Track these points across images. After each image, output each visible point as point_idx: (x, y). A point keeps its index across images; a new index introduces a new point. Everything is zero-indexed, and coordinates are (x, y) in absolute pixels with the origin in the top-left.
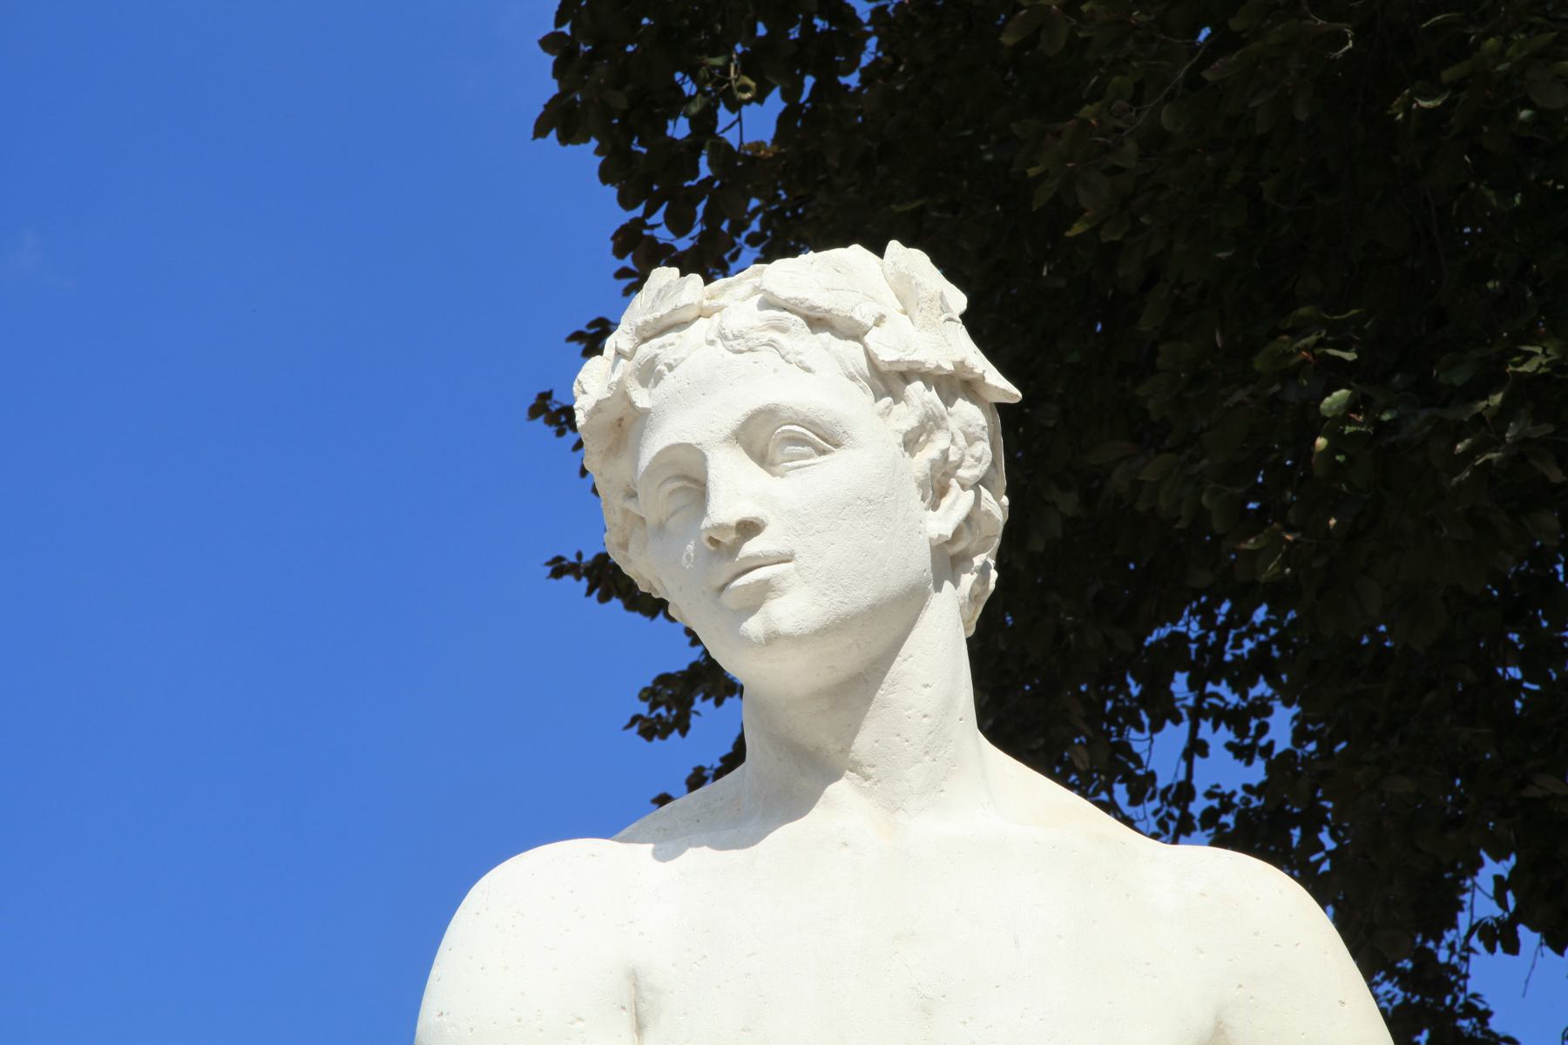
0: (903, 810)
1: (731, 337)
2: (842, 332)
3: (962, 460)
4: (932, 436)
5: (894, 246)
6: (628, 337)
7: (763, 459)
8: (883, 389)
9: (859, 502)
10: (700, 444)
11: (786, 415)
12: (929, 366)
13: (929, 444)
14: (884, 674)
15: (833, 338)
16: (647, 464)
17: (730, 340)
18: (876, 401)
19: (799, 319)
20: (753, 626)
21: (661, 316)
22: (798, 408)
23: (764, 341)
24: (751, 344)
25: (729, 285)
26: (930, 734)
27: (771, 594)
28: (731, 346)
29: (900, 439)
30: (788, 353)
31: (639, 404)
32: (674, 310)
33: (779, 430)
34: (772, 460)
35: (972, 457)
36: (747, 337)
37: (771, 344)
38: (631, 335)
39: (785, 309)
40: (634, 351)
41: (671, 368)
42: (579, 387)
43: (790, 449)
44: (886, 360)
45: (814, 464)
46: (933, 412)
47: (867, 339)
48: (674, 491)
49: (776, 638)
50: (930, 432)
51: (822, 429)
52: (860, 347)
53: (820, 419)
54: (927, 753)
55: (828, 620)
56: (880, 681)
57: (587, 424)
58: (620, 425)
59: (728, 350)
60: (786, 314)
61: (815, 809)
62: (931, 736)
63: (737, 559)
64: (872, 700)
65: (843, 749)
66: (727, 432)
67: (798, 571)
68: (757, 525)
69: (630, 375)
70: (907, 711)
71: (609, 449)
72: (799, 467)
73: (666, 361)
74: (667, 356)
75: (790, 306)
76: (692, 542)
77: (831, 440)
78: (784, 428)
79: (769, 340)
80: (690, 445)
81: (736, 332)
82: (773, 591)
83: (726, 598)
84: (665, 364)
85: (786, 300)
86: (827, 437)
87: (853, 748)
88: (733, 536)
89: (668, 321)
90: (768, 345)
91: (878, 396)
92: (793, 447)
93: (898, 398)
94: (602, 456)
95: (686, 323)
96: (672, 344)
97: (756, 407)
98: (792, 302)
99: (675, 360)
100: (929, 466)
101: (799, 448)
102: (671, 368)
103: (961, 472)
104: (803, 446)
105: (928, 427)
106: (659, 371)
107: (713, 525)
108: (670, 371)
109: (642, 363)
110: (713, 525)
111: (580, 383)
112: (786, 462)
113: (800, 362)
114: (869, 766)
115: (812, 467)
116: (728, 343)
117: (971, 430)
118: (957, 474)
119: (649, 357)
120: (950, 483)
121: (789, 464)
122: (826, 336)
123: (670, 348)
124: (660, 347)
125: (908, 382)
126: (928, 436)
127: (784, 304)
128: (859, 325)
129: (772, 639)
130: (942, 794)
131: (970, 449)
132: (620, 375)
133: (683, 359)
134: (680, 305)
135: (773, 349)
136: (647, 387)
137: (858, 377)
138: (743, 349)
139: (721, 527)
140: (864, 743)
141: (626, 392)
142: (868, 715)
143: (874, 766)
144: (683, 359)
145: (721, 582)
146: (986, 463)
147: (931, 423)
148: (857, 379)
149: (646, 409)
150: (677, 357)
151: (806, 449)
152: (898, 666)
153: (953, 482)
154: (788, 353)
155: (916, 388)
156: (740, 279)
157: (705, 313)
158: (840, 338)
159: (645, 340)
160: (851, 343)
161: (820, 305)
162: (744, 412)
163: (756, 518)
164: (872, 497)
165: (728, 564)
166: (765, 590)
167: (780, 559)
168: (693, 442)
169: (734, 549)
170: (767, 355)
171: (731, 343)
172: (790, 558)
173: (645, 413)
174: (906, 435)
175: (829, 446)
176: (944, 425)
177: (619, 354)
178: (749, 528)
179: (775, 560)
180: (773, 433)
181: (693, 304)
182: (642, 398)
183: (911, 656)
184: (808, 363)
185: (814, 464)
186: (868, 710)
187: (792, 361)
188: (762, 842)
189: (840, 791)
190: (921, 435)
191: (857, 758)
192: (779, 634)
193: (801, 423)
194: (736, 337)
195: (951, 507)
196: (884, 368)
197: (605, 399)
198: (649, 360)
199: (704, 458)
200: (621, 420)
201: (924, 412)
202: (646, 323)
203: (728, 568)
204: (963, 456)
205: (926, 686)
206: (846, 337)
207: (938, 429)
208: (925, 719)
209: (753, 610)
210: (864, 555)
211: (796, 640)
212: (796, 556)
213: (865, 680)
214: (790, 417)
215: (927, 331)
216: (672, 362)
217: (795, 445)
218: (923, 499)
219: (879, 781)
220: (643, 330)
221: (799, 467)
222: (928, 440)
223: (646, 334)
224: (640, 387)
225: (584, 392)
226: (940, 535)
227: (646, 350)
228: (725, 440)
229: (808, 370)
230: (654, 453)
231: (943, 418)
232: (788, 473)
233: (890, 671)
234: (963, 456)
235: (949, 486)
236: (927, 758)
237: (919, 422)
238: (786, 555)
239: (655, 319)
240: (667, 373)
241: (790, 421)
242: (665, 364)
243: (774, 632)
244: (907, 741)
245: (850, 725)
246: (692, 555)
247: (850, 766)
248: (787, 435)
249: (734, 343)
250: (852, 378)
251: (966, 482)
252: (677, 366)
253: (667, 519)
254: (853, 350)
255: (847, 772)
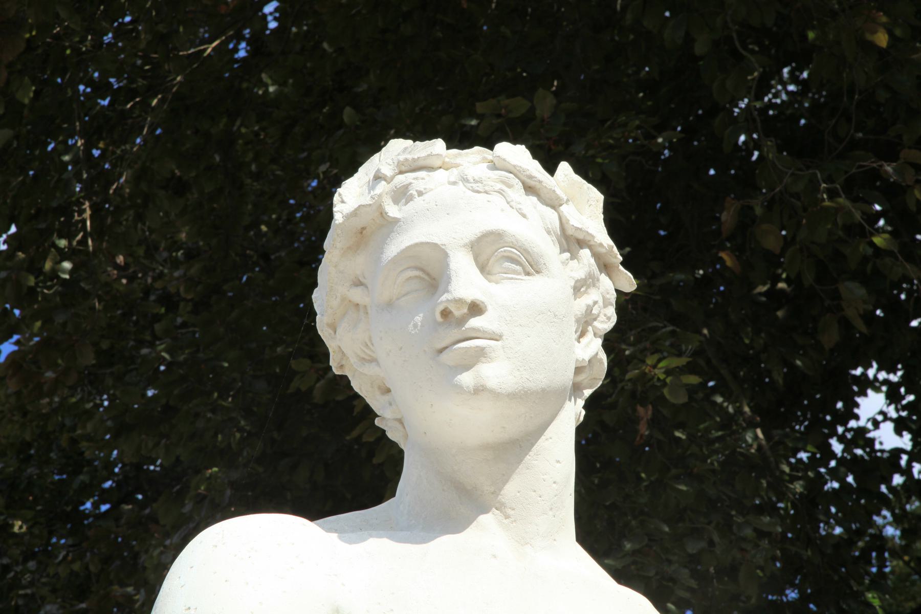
0: (531, 545)
1: (472, 181)
2: (544, 200)
3: (598, 315)
4: (589, 290)
5: (564, 168)
6: (390, 167)
7: (483, 268)
8: (566, 247)
9: (549, 313)
10: (445, 245)
11: (510, 240)
12: (596, 241)
13: (585, 295)
14: (533, 445)
15: (538, 202)
16: (394, 253)
17: (471, 183)
18: (560, 254)
19: (520, 183)
20: (466, 379)
21: (418, 158)
22: (519, 237)
23: (497, 189)
24: (487, 188)
25: (460, 155)
26: (555, 496)
27: (483, 359)
28: (472, 187)
29: (572, 284)
30: (512, 201)
31: (391, 214)
32: (429, 155)
33: (502, 250)
34: (489, 271)
35: (605, 315)
36: (485, 183)
37: (500, 192)
38: (392, 166)
39: (511, 173)
40: (393, 178)
41: (420, 194)
42: (338, 198)
43: (507, 264)
44: (575, 226)
45: (522, 280)
46: (594, 273)
47: (563, 208)
48: (410, 278)
49: (483, 390)
50: (588, 287)
51: (531, 256)
52: (556, 214)
53: (531, 250)
54: (551, 509)
55: (517, 388)
56: (530, 450)
57: (343, 223)
58: (361, 233)
59: (469, 189)
60: (512, 175)
61: (468, 530)
62: (556, 498)
63: (464, 328)
64: (522, 461)
65: (495, 491)
66: (467, 241)
67: (503, 348)
68: (481, 309)
69: (386, 194)
70: (543, 475)
71: (349, 248)
72: (512, 279)
73: (418, 189)
74: (418, 185)
75: (515, 171)
76: (421, 315)
77: (535, 266)
78: (506, 248)
79: (500, 189)
80: (436, 245)
81: (476, 178)
82: (485, 357)
83: (445, 356)
84: (417, 191)
85: (514, 166)
86: (533, 263)
87: (502, 492)
88: (465, 310)
89: (421, 163)
90: (499, 192)
91: (563, 251)
92: (510, 264)
93: (574, 257)
94: (342, 252)
95: (433, 168)
96: (423, 179)
97: (490, 229)
98: (518, 168)
99: (425, 189)
100: (585, 309)
101: (514, 265)
102: (420, 194)
103: (596, 323)
104: (517, 265)
105: (588, 283)
106: (411, 195)
107: (454, 298)
108: (419, 196)
109: (398, 187)
110: (454, 298)
111: (340, 195)
112: (502, 273)
113: (520, 209)
114: (510, 508)
115: (520, 281)
116: (469, 185)
117: (608, 296)
118: (594, 324)
119: (405, 183)
120: (588, 329)
121: (505, 275)
122: (534, 199)
123: (421, 180)
124: (414, 179)
125: (582, 248)
126: (586, 289)
127: (513, 169)
128: (558, 198)
129: (479, 390)
130: (555, 542)
131: (605, 309)
132: (381, 191)
133: (432, 190)
134: (434, 153)
135: (502, 196)
136: (398, 205)
137: (552, 232)
138: (481, 190)
139: (459, 301)
140: (511, 490)
141: (381, 205)
142: (517, 471)
143: (514, 509)
144: (432, 190)
145: (443, 344)
146: (612, 323)
147: (591, 280)
148: (551, 234)
149: (396, 218)
150: (427, 187)
151: (518, 268)
152: (542, 442)
153: (590, 328)
154: (512, 201)
155: (585, 253)
156: (467, 153)
157: (445, 167)
158: (542, 204)
159: (401, 173)
160: (549, 209)
161: (536, 176)
162: (481, 231)
163: (483, 303)
164: (557, 313)
165: (456, 331)
166: (480, 355)
167: (492, 337)
168: (439, 243)
169: (462, 321)
170: (496, 198)
171: (471, 185)
172: (498, 338)
173: (396, 221)
174: (577, 281)
175: (532, 270)
176: (597, 285)
177: (378, 177)
178: (476, 309)
179: (489, 337)
180: (496, 251)
181: (441, 155)
182: (393, 211)
183: (551, 438)
184: (525, 211)
185: (522, 280)
186: (518, 467)
187: (514, 207)
188: (432, 542)
189: (487, 520)
190: (582, 287)
191: (503, 500)
192: (486, 388)
193: (519, 249)
194: (476, 181)
195: (587, 345)
196: (570, 232)
197: (367, 205)
198: (404, 186)
199: (446, 255)
200: (363, 229)
201: (589, 271)
202: (406, 160)
203: (455, 334)
204: (600, 312)
205: (558, 462)
206: (547, 205)
207: (594, 286)
208: (554, 485)
209: (467, 368)
210: (546, 351)
211: (496, 395)
212: (504, 337)
213: (520, 445)
214: (512, 242)
215: (592, 220)
216: (422, 190)
217: (512, 263)
218: (576, 332)
219: (515, 521)
220: (403, 165)
221: (512, 279)
222: (585, 292)
223: (403, 168)
224: (392, 203)
225: (343, 202)
226: (583, 359)
227: (402, 179)
228: (465, 246)
229: (524, 216)
230: (403, 246)
231: (598, 280)
232: (502, 281)
233: (537, 444)
234: (600, 312)
235: (587, 331)
236: (551, 513)
237: (585, 276)
238: (497, 335)
239: (413, 159)
240: (416, 196)
241: (511, 245)
242: (417, 191)
243: (482, 386)
244: (540, 497)
245: (504, 475)
246: (420, 324)
247: (497, 505)
248: (505, 254)
249: (474, 185)
250: (549, 233)
251: (597, 331)
252: (426, 193)
253: (398, 299)
254: (551, 216)
255: (494, 509)
